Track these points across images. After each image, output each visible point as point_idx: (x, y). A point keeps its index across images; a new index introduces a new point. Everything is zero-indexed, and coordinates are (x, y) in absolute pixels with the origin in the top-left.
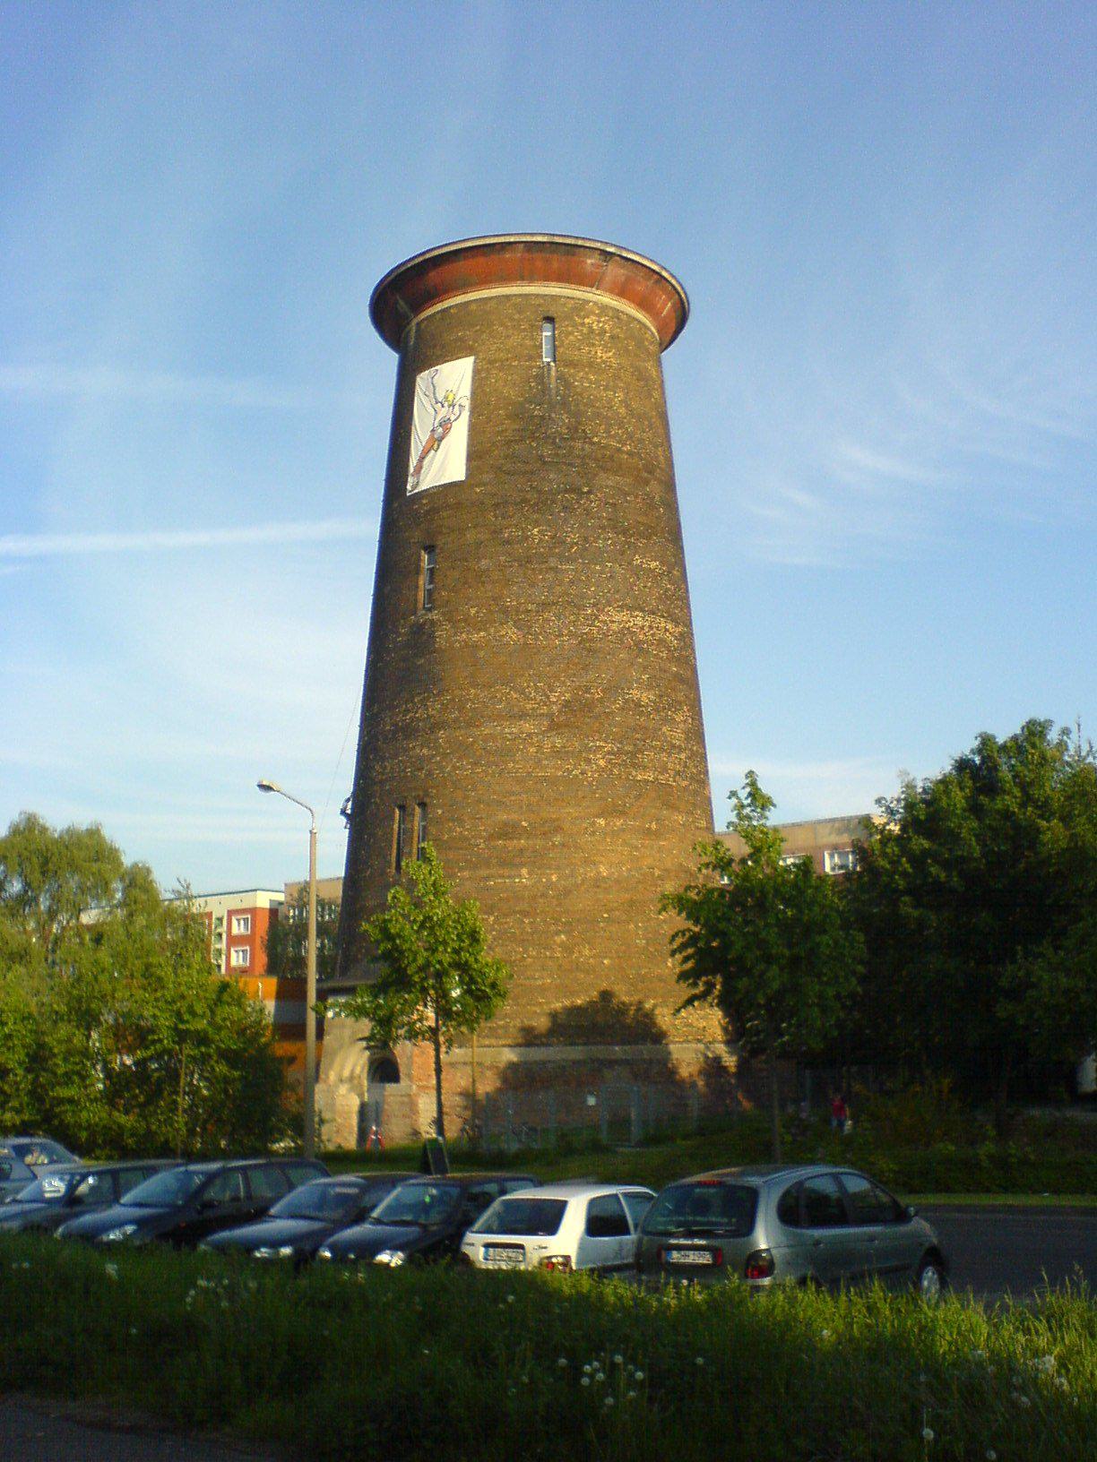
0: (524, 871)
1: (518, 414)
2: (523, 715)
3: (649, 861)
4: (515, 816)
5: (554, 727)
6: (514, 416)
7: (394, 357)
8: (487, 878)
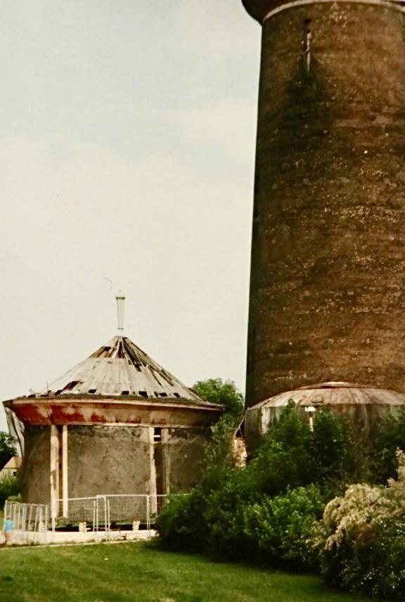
0: (290, 372)
1: (291, 89)
2: (290, 279)
3: (365, 364)
4: (286, 339)
5: (306, 284)
6: (287, 91)
7: (256, 29)
8: (274, 377)
